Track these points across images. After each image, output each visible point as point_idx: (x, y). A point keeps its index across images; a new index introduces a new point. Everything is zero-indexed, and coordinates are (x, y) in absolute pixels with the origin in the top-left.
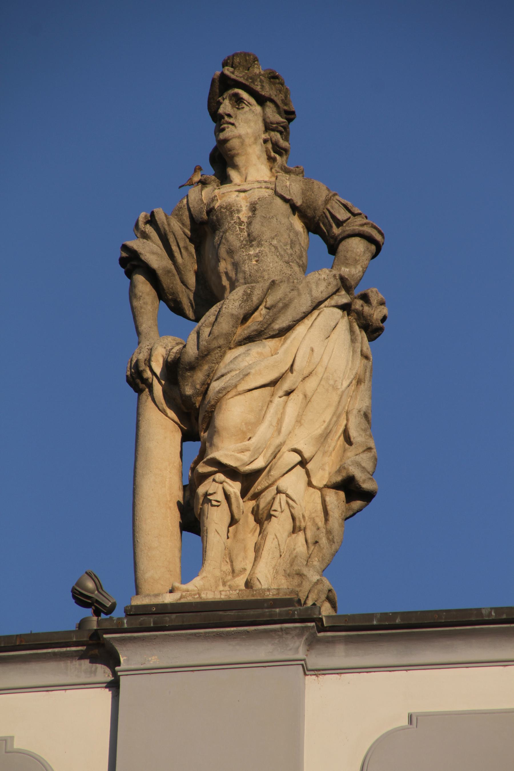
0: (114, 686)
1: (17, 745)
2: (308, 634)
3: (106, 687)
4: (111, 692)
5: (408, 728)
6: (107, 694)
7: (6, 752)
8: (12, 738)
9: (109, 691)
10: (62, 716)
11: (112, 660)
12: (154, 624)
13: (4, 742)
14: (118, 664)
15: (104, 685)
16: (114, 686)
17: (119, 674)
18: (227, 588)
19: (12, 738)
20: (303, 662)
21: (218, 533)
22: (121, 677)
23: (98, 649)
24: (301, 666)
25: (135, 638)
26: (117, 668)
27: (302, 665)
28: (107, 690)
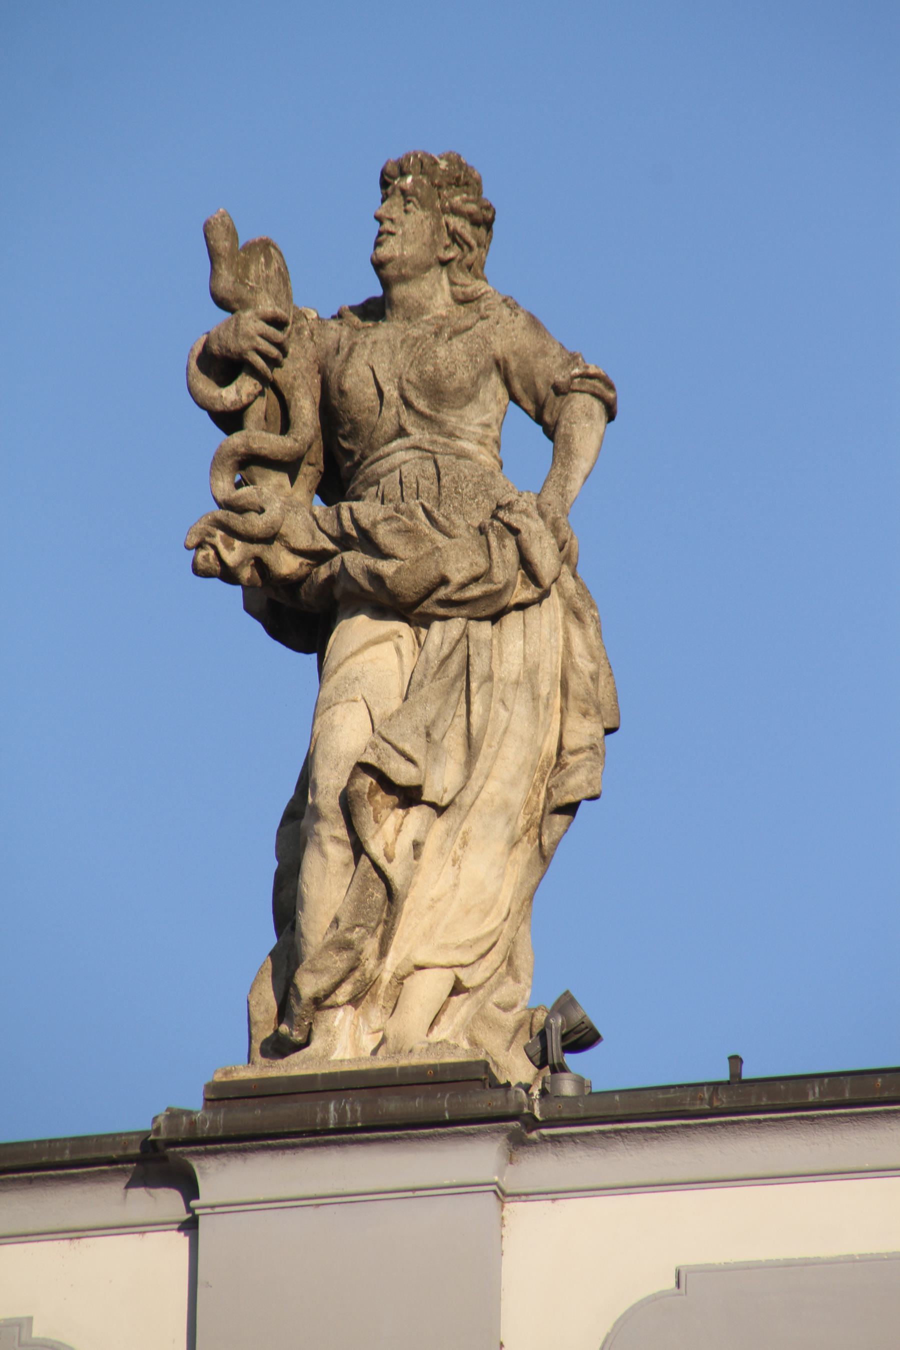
0: (190, 1226)
1: (38, 1332)
2: (349, 1120)
3: (179, 1230)
4: (187, 1239)
5: (676, 1295)
6: (182, 1241)
7: (20, 1345)
8: (30, 1320)
9: (185, 1235)
10: (106, 1285)
11: (189, 1188)
12: (71, 1152)
13: (17, 1329)
14: (196, 1196)
15: (176, 1226)
16: (190, 1226)
17: (197, 1212)
18: (452, 357)
19: (30, 1320)
20: (494, 1187)
21: (316, 705)
22: (201, 1218)
23: (160, 1161)
24: (492, 1194)
25: (52, 1178)
26: (193, 1203)
27: (495, 1192)
28: (182, 1234)
